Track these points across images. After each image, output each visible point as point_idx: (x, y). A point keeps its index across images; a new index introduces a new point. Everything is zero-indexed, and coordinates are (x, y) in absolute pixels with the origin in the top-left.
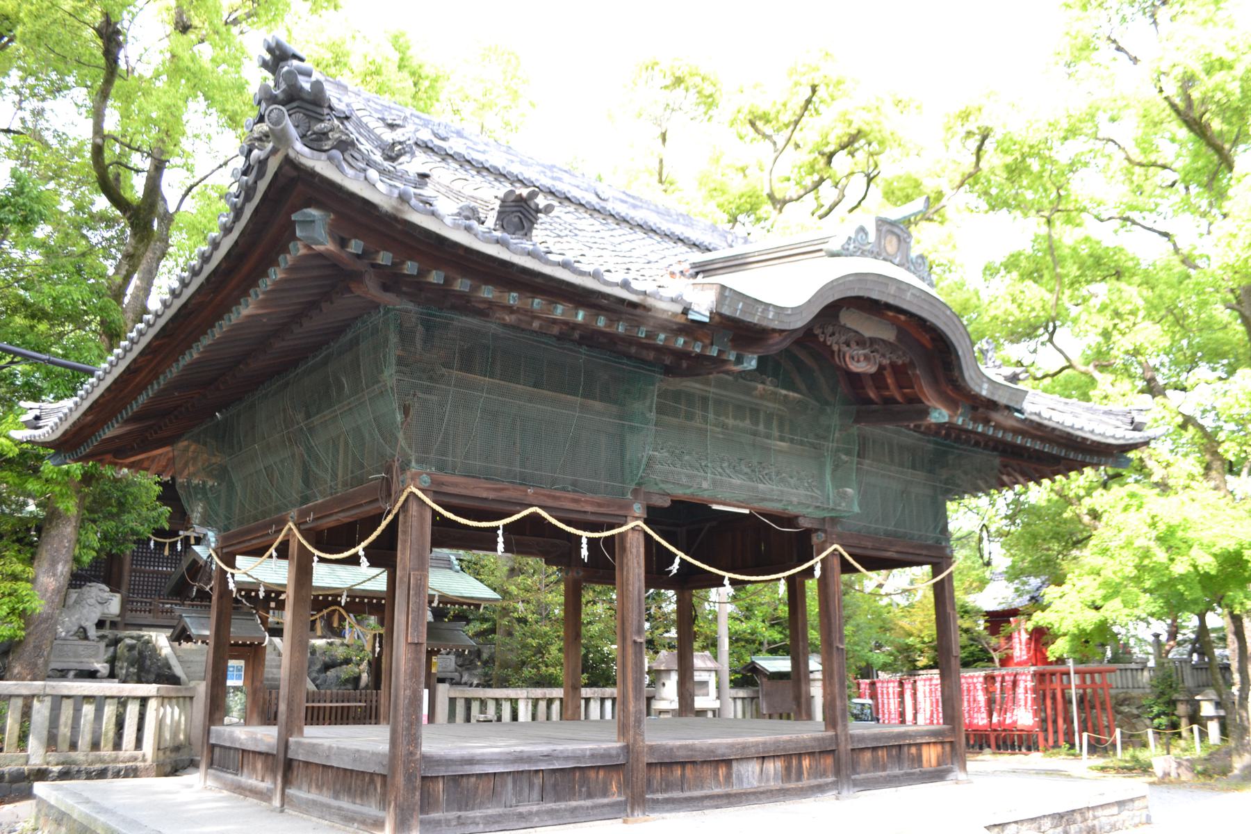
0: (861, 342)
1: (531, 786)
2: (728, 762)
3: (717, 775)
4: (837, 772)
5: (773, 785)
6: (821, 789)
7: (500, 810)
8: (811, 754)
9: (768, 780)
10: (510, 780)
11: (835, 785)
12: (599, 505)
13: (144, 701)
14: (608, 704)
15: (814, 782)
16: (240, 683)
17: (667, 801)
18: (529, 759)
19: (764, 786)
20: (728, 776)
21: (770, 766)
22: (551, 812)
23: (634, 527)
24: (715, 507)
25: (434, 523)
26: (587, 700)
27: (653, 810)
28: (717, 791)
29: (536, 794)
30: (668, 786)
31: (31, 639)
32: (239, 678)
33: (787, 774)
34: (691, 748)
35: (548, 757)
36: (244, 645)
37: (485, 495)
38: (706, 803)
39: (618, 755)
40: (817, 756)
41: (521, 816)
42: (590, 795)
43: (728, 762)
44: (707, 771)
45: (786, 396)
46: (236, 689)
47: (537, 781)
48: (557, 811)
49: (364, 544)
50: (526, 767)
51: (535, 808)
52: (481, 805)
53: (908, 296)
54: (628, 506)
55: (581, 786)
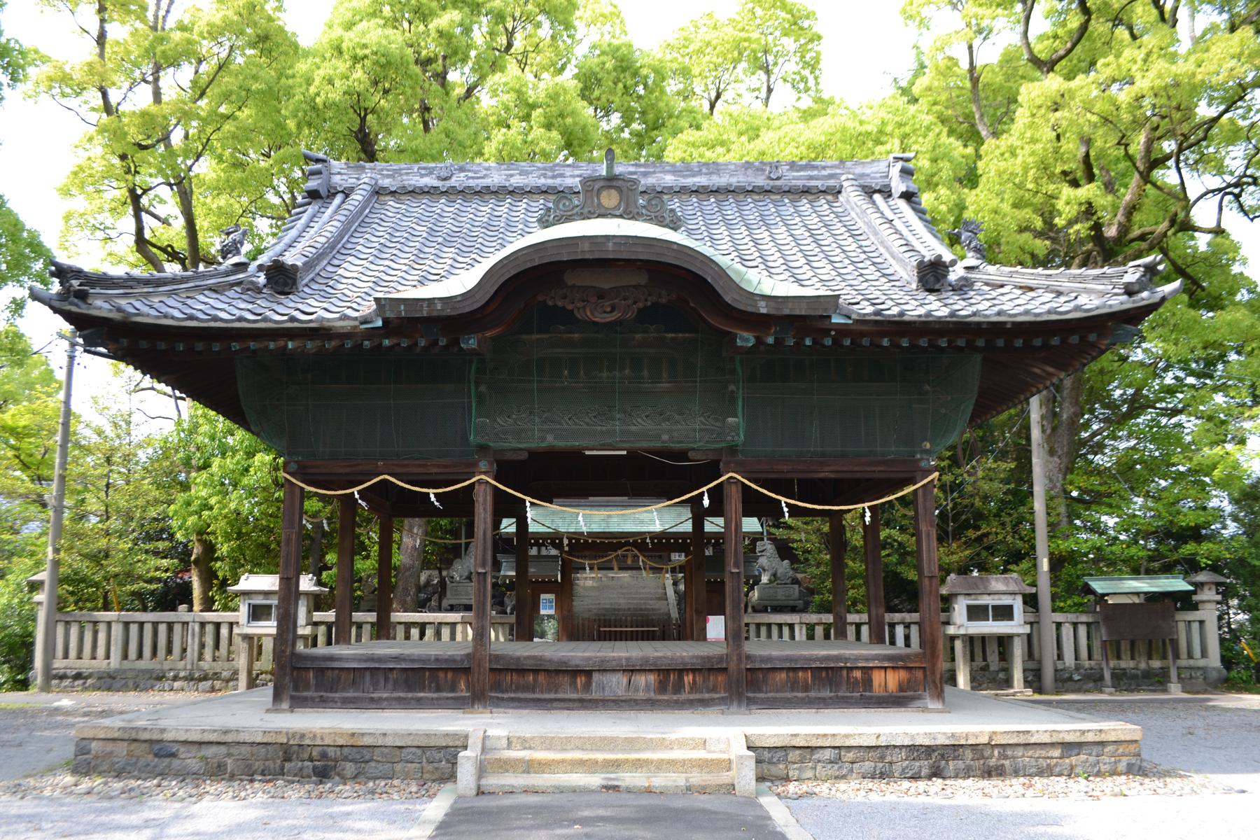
0: (601, 295)
1: (386, 679)
2: (588, 673)
3: (575, 682)
4: (728, 688)
5: (641, 695)
6: (704, 703)
7: (361, 695)
8: (694, 671)
9: (637, 690)
10: (368, 674)
11: (722, 701)
12: (446, 467)
13: (453, 625)
14: (1082, 631)
15: (692, 697)
16: (552, 612)
17: (512, 699)
18: (380, 659)
19: (631, 695)
20: (587, 686)
21: (641, 680)
22: (399, 699)
23: (484, 479)
24: (587, 453)
26: (892, 626)
27: (498, 706)
28: (574, 696)
29: (390, 685)
30: (519, 688)
31: (400, 583)
32: (551, 608)
33: (662, 687)
34: (541, 659)
35: (397, 658)
36: (543, 581)
37: (341, 471)
38: (555, 705)
39: (462, 661)
40: (232, 648)
41: (372, 700)
42: (438, 690)
43: (588, 673)
45: (672, 339)
46: (549, 617)
47: (394, 675)
48: (405, 699)
50: (377, 665)
51: (385, 695)
52: (344, 690)
54: (475, 464)
55: (430, 683)
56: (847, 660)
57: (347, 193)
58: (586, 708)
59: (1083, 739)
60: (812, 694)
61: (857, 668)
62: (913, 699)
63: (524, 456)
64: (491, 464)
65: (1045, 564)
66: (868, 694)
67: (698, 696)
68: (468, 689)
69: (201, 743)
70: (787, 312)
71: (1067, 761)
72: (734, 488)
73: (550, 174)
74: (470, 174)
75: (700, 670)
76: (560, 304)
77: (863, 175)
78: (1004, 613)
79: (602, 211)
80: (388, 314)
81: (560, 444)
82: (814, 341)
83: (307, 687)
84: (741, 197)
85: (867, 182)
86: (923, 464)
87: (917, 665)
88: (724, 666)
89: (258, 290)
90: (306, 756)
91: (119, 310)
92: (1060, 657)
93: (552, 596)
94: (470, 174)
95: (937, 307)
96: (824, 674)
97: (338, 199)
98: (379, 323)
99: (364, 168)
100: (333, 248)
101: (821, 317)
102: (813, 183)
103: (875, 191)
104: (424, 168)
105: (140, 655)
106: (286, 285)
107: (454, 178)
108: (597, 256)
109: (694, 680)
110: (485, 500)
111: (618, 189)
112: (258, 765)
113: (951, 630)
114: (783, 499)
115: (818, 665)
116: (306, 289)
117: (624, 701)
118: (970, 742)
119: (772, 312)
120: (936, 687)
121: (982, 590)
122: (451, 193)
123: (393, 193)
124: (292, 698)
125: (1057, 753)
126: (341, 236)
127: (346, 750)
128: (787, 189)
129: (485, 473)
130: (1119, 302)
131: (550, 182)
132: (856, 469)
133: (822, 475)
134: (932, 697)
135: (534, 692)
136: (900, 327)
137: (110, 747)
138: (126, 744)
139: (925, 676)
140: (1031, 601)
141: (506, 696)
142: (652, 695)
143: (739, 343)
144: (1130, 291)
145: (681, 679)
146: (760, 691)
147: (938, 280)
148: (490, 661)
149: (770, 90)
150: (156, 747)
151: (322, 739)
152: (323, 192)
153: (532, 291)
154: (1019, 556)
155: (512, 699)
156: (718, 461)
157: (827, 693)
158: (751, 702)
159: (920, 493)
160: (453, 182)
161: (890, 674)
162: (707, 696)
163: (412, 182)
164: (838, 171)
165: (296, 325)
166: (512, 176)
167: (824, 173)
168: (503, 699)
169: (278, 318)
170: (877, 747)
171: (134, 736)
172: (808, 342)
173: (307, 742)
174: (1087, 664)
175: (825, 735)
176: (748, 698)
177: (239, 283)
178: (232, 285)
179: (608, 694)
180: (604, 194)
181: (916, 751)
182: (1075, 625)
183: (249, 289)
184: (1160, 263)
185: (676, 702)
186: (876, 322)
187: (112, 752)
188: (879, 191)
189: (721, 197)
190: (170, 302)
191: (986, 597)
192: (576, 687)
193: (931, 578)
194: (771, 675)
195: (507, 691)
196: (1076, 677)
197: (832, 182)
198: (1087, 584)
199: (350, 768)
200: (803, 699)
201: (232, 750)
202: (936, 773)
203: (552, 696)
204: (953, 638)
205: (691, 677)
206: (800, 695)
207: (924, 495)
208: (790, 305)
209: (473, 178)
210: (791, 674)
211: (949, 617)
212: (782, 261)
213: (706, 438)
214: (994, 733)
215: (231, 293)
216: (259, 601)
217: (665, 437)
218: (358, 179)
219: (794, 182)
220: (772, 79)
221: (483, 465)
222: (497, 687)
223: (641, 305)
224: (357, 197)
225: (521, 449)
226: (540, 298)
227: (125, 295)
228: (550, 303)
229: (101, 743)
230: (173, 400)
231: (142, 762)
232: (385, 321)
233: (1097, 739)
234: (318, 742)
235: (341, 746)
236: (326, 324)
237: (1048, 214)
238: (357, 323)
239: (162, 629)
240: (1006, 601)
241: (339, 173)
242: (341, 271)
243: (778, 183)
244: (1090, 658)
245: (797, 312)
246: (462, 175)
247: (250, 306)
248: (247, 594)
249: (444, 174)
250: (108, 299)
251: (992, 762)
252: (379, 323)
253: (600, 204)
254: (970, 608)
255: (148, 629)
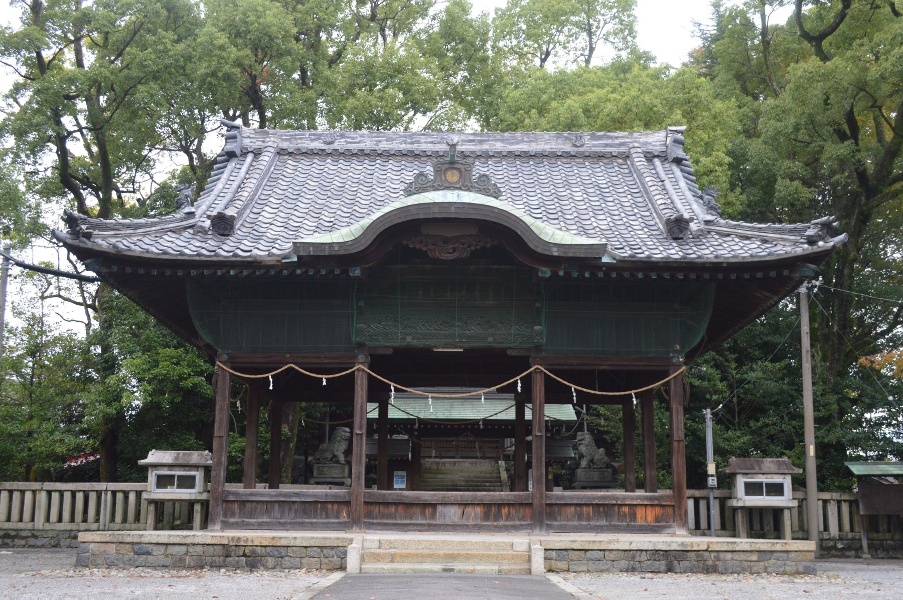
0: (446, 241)
1: (290, 509)
5: (471, 522)
8: (509, 505)
9: (468, 519)
14: (845, 508)
15: (507, 523)
17: (379, 524)
20: (433, 516)
23: (361, 369)
25: (232, 380)
27: (369, 528)
28: (424, 522)
29: (293, 514)
30: (384, 516)
33: (486, 517)
38: (410, 528)
39: (345, 497)
41: (280, 523)
42: (327, 517)
44: (417, 510)
47: (296, 506)
49: (273, 373)
53: (453, 209)
54: (356, 357)
55: (321, 512)
56: (618, 499)
57: (257, 153)
58: (433, 530)
59: (773, 549)
60: (593, 523)
61: (625, 505)
62: (665, 527)
63: (390, 352)
64: (366, 357)
65: (811, 451)
66: (633, 523)
67: (511, 523)
68: (348, 516)
69: (167, 545)
70: (571, 255)
71: (762, 563)
72: (538, 376)
73: (409, 140)
74: (349, 140)
75: (513, 505)
76: (418, 247)
77: (646, 143)
78: (776, 489)
79: (447, 185)
80: (302, 253)
81: (415, 343)
82: (591, 274)
83: (233, 515)
84: (553, 160)
85: (650, 148)
86: (675, 360)
87: (668, 503)
88: (530, 501)
89: (204, 231)
90: (241, 553)
91: (115, 246)
92: (826, 528)
93: (404, 473)
94: (349, 140)
95: (675, 252)
96: (601, 509)
97: (250, 157)
98: (295, 259)
99: (268, 133)
100: (252, 200)
101: (595, 258)
102: (609, 149)
103: (655, 156)
104: (314, 135)
105: (60, 520)
106: (226, 229)
107: (336, 143)
108: (444, 216)
109: (509, 512)
110: (362, 383)
111: (459, 170)
112: (209, 559)
113: (735, 503)
114: (573, 387)
115: (597, 502)
116: (239, 232)
117: (459, 526)
118: (694, 549)
119: (562, 255)
120: (682, 519)
121: (757, 470)
122: (337, 155)
123: (290, 154)
124: (222, 522)
125: (754, 557)
126: (257, 190)
127: (269, 549)
128: (587, 154)
129: (362, 363)
130: (803, 249)
131: (409, 147)
132: (627, 363)
133: (602, 368)
134: (679, 526)
135: (396, 519)
136: (648, 265)
137: (103, 547)
138: (114, 545)
139: (674, 512)
140: (799, 483)
141: (375, 521)
142: (479, 522)
143: (540, 274)
144: (811, 241)
145: (499, 511)
146: (556, 520)
147: (681, 232)
148: (364, 496)
149: (592, 50)
150: (136, 547)
151: (252, 541)
152: (238, 152)
153: (402, 242)
154: (790, 443)
155: (379, 524)
156: (529, 357)
157: (604, 522)
158: (549, 527)
159: (672, 381)
160: (336, 146)
161: (649, 510)
162: (518, 523)
163: (305, 146)
164: (627, 140)
165: (238, 259)
166: (380, 141)
167: (617, 141)
168: (373, 523)
169: (225, 254)
170: (630, 550)
171: (121, 540)
172: (587, 275)
173: (242, 543)
174: (850, 535)
175: (594, 542)
176: (547, 525)
177: (191, 227)
178: (186, 228)
179: (448, 521)
180: (449, 173)
181: (655, 554)
182: (839, 502)
183: (199, 232)
184: (833, 221)
185: (496, 527)
186: (633, 261)
187: (105, 551)
188: (658, 156)
189: (538, 160)
190: (146, 240)
191: (761, 476)
192: (425, 515)
193: (679, 441)
194: (563, 509)
195: (376, 518)
196: (840, 546)
197: (622, 149)
198: (847, 468)
199: (271, 561)
200: (586, 526)
201: (190, 549)
202: (670, 569)
203: (408, 522)
204: (735, 510)
205: (506, 509)
206: (584, 523)
207: (675, 382)
208: (573, 250)
209: (350, 143)
210: (578, 509)
211: (731, 494)
212: (575, 214)
213: (520, 340)
214: (712, 543)
215: (186, 234)
216: (165, 472)
217: (490, 339)
218: (263, 142)
219: (594, 149)
220: (595, 39)
221: (361, 358)
222: (369, 515)
223: (473, 248)
224: (266, 158)
225: (388, 347)
226: (404, 243)
227: (115, 236)
228: (411, 246)
229: (97, 545)
230: (83, 308)
231: (126, 558)
232: (299, 257)
233: (783, 549)
234: (250, 543)
235: (265, 546)
236: (259, 259)
237: (813, 162)
238: (279, 258)
239: (80, 497)
240: (777, 479)
241: (249, 137)
242: (261, 218)
243: (581, 149)
244: (852, 530)
245: (578, 255)
246: (343, 140)
247: (203, 245)
248: (155, 466)
249: (329, 139)
250: (104, 238)
251: (710, 563)
252: (295, 259)
253: (446, 179)
254: (747, 485)
255: (67, 496)
